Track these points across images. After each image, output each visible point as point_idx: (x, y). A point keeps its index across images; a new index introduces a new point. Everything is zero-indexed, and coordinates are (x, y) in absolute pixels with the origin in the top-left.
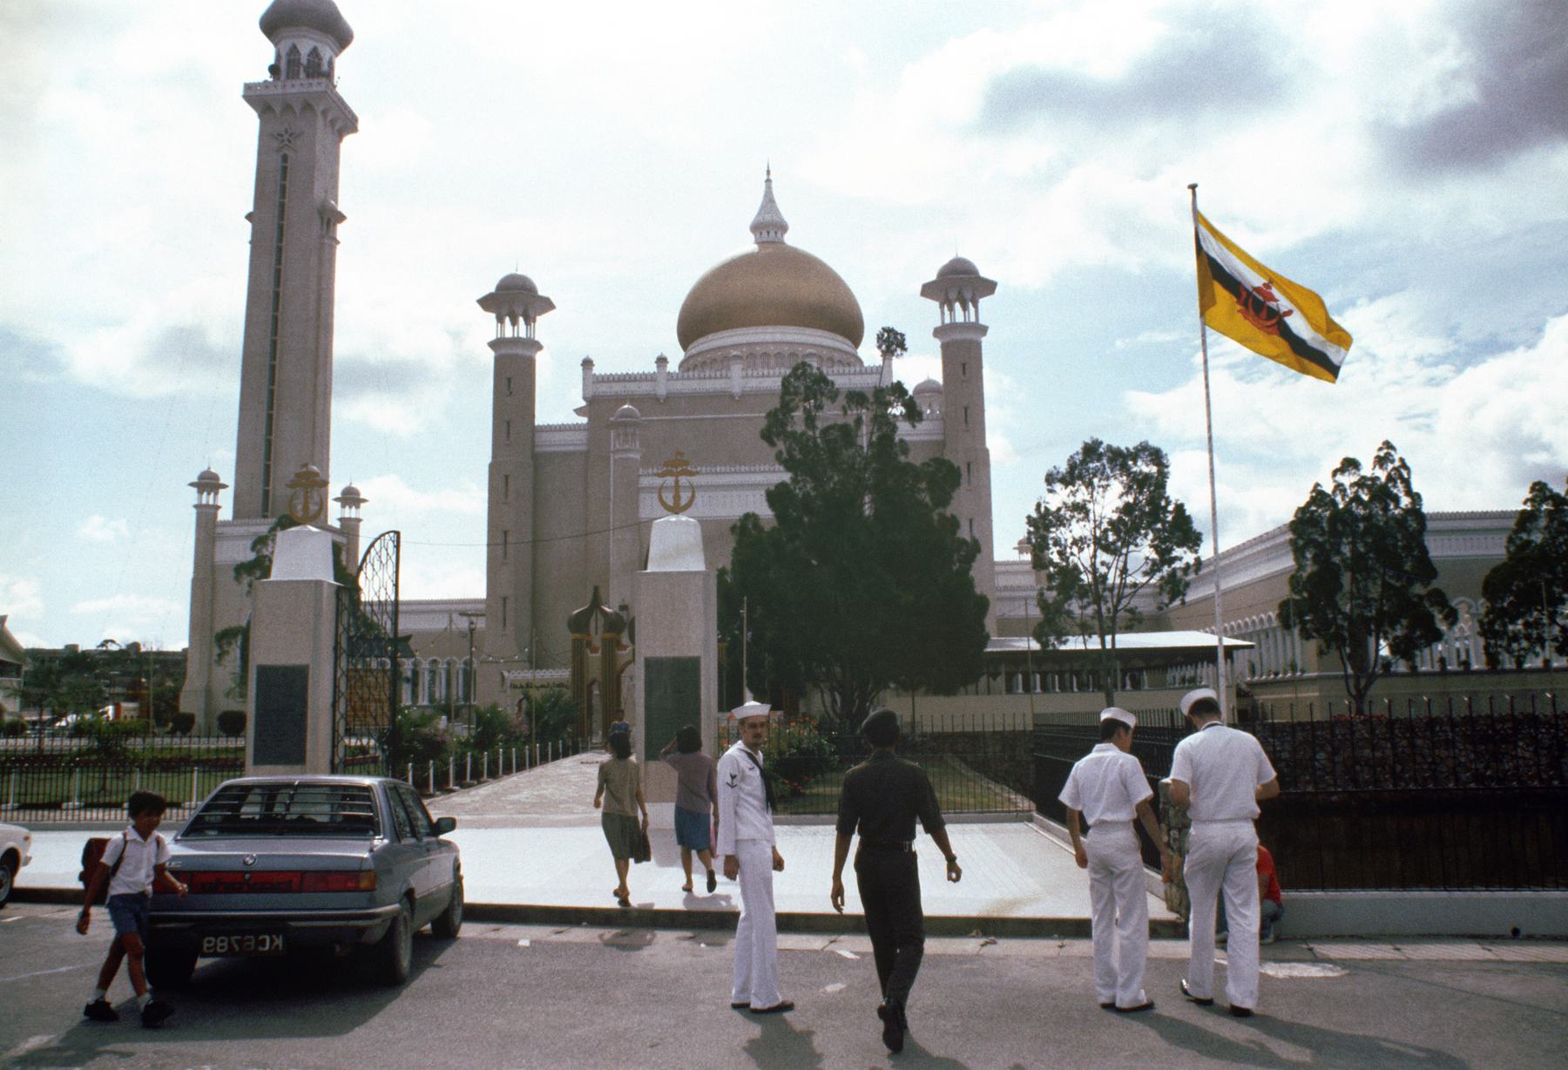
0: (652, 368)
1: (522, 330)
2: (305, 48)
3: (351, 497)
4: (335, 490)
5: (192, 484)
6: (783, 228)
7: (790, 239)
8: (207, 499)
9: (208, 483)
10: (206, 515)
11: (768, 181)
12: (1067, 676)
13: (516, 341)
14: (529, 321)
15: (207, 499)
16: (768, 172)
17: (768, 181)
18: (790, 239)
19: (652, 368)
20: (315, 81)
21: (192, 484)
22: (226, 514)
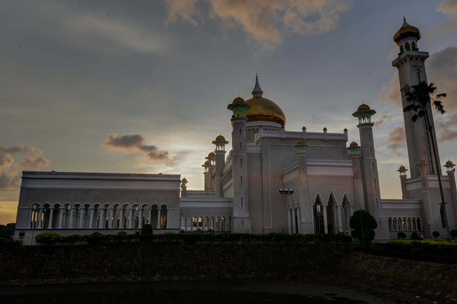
0: (301, 131)
1: (367, 121)
2: (410, 42)
3: (449, 164)
4: (443, 163)
5: (398, 171)
6: (261, 93)
7: (263, 96)
8: (403, 174)
9: (402, 169)
10: (403, 179)
11: (257, 80)
12: (406, 182)
13: (366, 124)
14: (369, 118)
15: (403, 174)
16: (257, 77)
17: (257, 80)
18: (263, 96)
19: (301, 131)
20: (414, 52)
21: (398, 171)
22: (409, 176)
